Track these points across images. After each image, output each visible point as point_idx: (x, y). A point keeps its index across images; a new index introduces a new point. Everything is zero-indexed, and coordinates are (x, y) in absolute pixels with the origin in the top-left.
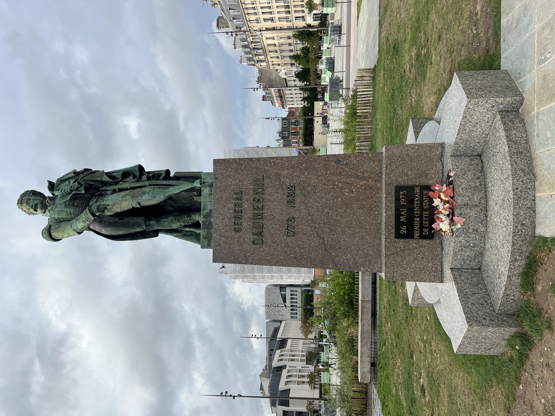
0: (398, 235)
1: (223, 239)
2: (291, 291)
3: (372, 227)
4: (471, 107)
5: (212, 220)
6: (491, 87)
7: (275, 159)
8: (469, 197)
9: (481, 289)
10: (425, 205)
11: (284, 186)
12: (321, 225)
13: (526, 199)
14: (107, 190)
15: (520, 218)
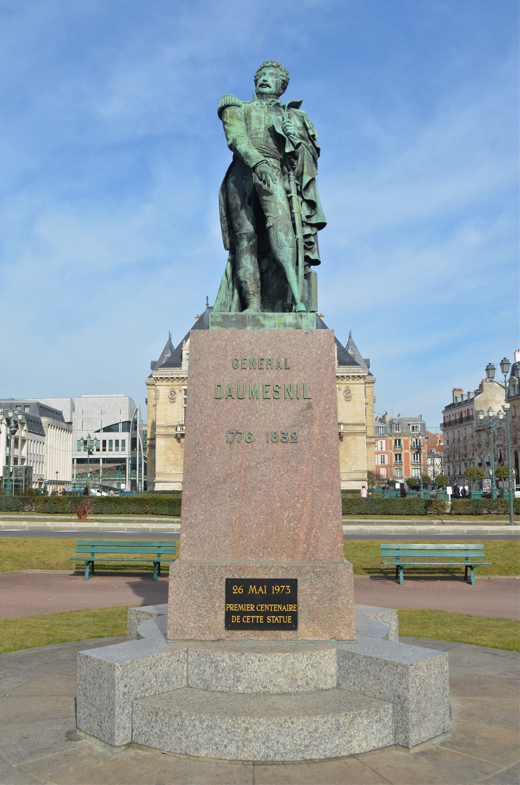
0: (230, 583)
1: (224, 343)
2: (124, 441)
3: (241, 549)
4: (399, 670)
5: (249, 328)
6: (425, 696)
7: (334, 415)
8: (283, 671)
9: (162, 686)
10: (271, 619)
11: (298, 428)
12: (243, 480)
13: (280, 733)
14: (289, 181)
15: (255, 726)
